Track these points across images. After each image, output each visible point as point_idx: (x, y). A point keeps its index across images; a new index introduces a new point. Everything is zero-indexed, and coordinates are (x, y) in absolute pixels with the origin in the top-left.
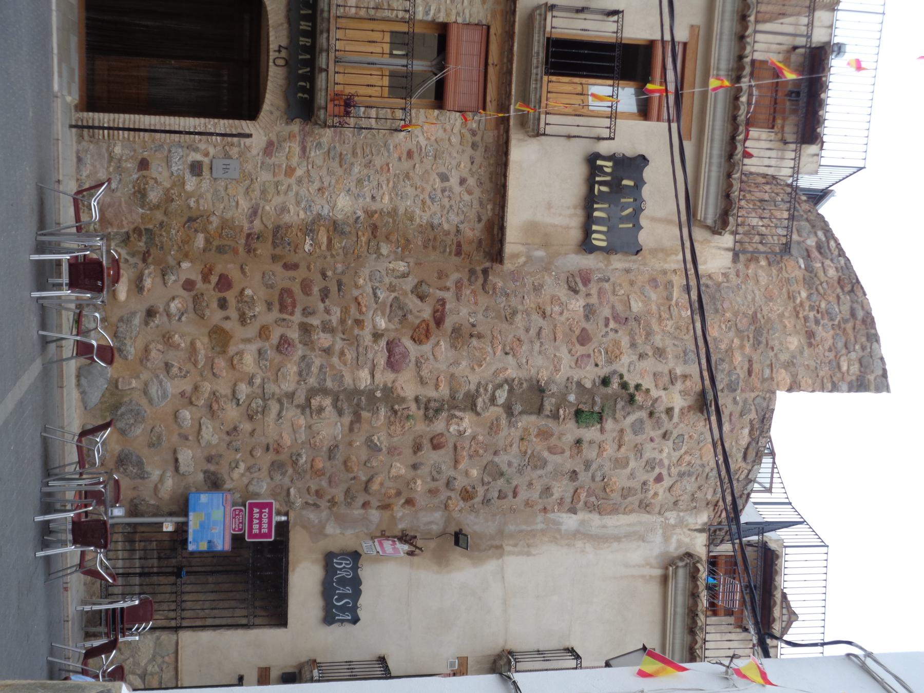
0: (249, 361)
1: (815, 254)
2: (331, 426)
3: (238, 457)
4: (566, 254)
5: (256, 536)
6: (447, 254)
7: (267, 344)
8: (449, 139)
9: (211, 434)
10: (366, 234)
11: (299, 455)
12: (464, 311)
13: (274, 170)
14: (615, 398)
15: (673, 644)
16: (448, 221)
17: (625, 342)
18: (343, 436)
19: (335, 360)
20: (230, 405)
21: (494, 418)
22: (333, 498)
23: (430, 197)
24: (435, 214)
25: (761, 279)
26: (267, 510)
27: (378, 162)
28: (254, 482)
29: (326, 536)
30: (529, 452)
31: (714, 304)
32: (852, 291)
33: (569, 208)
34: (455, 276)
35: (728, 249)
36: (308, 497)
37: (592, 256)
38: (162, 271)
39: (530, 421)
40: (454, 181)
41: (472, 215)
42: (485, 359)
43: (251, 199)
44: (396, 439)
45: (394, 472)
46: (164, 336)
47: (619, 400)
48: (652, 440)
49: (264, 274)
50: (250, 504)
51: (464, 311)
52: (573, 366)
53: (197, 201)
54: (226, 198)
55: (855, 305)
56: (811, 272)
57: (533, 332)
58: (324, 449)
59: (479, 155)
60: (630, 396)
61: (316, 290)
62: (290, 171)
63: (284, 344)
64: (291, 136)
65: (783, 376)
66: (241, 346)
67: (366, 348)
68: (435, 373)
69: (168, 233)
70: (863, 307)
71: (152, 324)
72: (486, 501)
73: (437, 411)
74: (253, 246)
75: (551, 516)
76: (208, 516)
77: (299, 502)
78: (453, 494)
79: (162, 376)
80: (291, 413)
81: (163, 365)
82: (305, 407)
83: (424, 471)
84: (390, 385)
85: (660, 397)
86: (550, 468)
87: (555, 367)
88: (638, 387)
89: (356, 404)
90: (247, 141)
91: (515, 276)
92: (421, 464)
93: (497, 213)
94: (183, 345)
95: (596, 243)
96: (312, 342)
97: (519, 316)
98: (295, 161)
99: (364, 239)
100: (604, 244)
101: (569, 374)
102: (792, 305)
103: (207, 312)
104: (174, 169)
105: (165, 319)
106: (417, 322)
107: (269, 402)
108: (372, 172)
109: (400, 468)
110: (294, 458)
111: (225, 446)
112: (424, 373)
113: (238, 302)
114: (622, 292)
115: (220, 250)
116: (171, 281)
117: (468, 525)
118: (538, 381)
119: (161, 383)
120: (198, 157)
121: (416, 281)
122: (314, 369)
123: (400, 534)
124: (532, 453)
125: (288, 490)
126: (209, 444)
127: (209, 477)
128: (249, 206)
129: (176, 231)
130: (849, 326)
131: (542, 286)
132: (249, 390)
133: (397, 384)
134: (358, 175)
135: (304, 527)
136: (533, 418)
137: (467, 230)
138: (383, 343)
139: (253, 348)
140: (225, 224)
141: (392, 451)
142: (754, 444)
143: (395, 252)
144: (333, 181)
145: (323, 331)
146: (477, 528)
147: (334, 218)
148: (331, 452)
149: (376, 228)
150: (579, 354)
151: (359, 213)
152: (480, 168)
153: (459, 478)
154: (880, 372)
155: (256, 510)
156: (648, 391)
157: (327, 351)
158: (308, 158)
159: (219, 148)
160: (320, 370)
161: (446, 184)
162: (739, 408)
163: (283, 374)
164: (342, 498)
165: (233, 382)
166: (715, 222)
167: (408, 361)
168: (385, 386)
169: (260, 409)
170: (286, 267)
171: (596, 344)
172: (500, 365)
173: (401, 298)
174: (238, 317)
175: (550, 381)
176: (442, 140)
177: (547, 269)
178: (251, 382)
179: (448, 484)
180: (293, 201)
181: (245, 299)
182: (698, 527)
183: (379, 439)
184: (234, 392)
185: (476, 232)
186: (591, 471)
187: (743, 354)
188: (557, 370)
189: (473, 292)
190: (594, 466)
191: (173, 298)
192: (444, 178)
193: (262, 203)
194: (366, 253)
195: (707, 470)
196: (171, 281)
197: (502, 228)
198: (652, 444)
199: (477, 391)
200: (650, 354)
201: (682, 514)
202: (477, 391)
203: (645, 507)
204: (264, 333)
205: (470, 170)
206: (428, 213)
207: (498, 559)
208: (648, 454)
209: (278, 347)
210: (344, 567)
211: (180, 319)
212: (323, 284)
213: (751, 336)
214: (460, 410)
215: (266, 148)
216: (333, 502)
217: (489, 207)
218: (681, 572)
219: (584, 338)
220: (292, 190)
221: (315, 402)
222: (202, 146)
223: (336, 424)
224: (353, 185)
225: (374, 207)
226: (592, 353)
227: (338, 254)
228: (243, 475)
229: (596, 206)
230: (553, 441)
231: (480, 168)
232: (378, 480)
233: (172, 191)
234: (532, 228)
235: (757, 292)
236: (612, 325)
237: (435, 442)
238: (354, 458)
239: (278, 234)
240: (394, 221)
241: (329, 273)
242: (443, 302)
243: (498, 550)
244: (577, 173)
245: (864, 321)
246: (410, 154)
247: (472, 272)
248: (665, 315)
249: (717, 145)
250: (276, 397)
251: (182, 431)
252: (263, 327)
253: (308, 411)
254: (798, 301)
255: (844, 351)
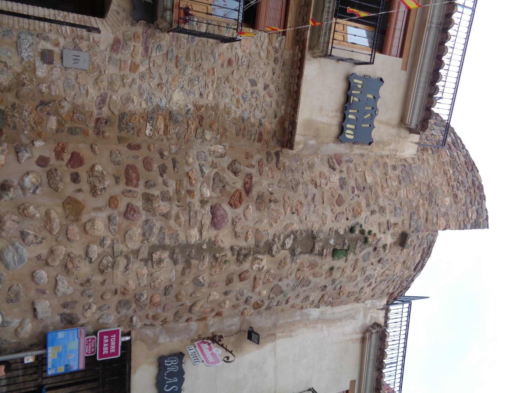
0: (100, 227)
1: (453, 147)
2: (167, 272)
3: (90, 300)
4: (328, 143)
5: (106, 355)
6: (252, 140)
7: (116, 212)
8: (259, 53)
9: (66, 287)
10: (195, 123)
11: (142, 295)
12: (265, 183)
13: (120, 64)
14: (356, 240)
15: (367, 377)
16: (254, 117)
17: (363, 203)
18: (176, 278)
19: (172, 222)
20: (83, 263)
21: (282, 258)
22: (165, 319)
23: (243, 97)
24: (246, 110)
25: (430, 162)
26: (115, 336)
27: (206, 66)
28: (104, 317)
29: (160, 344)
30: (302, 277)
31: (409, 178)
32: (472, 169)
33: (333, 111)
34: (257, 157)
35: (416, 143)
36: (146, 320)
37: (343, 145)
38: (16, 148)
39: (306, 258)
40: (260, 86)
41: (271, 113)
42: (279, 217)
43: (100, 89)
44: (215, 277)
45: (211, 298)
46: (19, 208)
47: (359, 241)
48: (372, 264)
49: (111, 152)
50: (101, 333)
51: (265, 183)
52: (334, 220)
53: (49, 87)
54: (77, 86)
55: (475, 179)
56: (453, 158)
57: (310, 198)
58: (162, 288)
59: (278, 67)
60: (365, 238)
61: (155, 166)
62: (134, 67)
63: (130, 212)
64: (135, 37)
65: (442, 222)
66: (93, 214)
67: (196, 213)
68: (245, 229)
69: (21, 114)
70: (478, 179)
71: (6, 197)
72: (269, 308)
73: (246, 256)
74: (102, 129)
75: (304, 311)
76: (65, 347)
77: (139, 324)
78: (248, 307)
79: (17, 244)
80: (136, 266)
81: (19, 233)
82: (148, 260)
83: (232, 295)
84: (213, 239)
85: (381, 238)
86: (311, 285)
87: (323, 221)
88: (370, 232)
89: (186, 254)
90: (96, 36)
91: (297, 158)
92: (230, 291)
93: (289, 111)
94: (38, 215)
95: (347, 136)
96: (154, 209)
97: (301, 186)
98: (138, 58)
99: (193, 127)
100: (352, 137)
101: (331, 226)
102: (446, 178)
103: (61, 186)
104: (25, 55)
105: (20, 192)
106: (233, 191)
107: (118, 259)
108: (201, 74)
109: (216, 295)
110: (137, 297)
111: (79, 294)
112: (238, 229)
113: (89, 176)
114: (360, 170)
115: (72, 131)
116: (25, 158)
117: (255, 323)
118: (312, 232)
119: (17, 250)
120: (49, 46)
121: (231, 160)
122: (156, 231)
123: (211, 335)
124: (303, 278)
125: (131, 318)
126: (65, 295)
127: (65, 318)
128: (98, 94)
129: (28, 112)
130: (472, 191)
131: (314, 165)
132: (101, 250)
133: (218, 239)
134: (190, 76)
135: (143, 340)
136: (307, 256)
137: (267, 124)
138: (208, 208)
139: (104, 215)
140: (75, 109)
141: (210, 285)
142: (422, 261)
143: (216, 138)
144: (170, 79)
145: (162, 200)
146: (260, 324)
147: (170, 109)
148: (166, 291)
149: (202, 119)
150: (337, 212)
151: (190, 106)
152: (279, 78)
153: (254, 297)
154: (485, 217)
155: (106, 337)
156: (375, 234)
157: (166, 216)
158: (150, 57)
159: (69, 40)
160: (160, 231)
161: (255, 88)
162: (419, 242)
163: (130, 235)
164: (172, 318)
165: (86, 244)
166: (417, 126)
167: (226, 221)
168: (210, 240)
169: (110, 265)
170: (130, 147)
171: (347, 205)
172: (289, 222)
173: (220, 173)
174: (89, 189)
175: (320, 231)
176: (254, 53)
177: (316, 153)
178: (102, 243)
179: (246, 301)
180: (137, 93)
181: (96, 174)
182: (381, 307)
183: (203, 278)
184: (87, 253)
185: (272, 125)
186: (335, 285)
187: (424, 209)
188: (324, 224)
189: (270, 169)
190: (337, 282)
191: (28, 174)
192: (254, 83)
193: (110, 93)
194: (194, 138)
195: (395, 277)
196: (25, 158)
197: (293, 124)
198: (372, 266)
199: (273, 240)
200: (377, 210)
201: (374, 301)
202: (273, 240)
203: (357, 300)
204: (112, 202)
205: (272, 79)
206: (241, 109)
207: (272, 342)
208: (367, 273)
209: (125, 215)
210: (172, 365)
211: (34, 192)
212: (161, 162)
213: (428, 197)
214: (261, 254)
215: (113, 45)
216: (165, 322)
217: (283, 107)
218: (374, 336)
219: (340, 202)
220: (136, 83)
221: (155, 256)
222: (53, 36)
223: (172, 270)
224: (186, 83)
225: (201, 102)
226: (345, 211)
227: (172, 138)
228: (94, 313)
229: (350, 111)
230: (317, 269)
231: (279, 78)
232: (200, 304)
233: (24, 76)
234: (309, 123)
235: (429, 170)
236: (356, 192)
237: (242, 276)
238: (183, 293)
239: (123, 120)
240: (216, 114)
241: (166, 153)
242: (250, 176)
243: (273, 336)
244: (340, 87)
245: (478, 188)
246: (230, 62)
247: (268, 154)
248: (385, 185)
249: (424, 75)
250: (124, 254)
251: (39, 287)
252: (112, 197)
253: (150, 263)
254: (449, 176)
255: (470, 206)
